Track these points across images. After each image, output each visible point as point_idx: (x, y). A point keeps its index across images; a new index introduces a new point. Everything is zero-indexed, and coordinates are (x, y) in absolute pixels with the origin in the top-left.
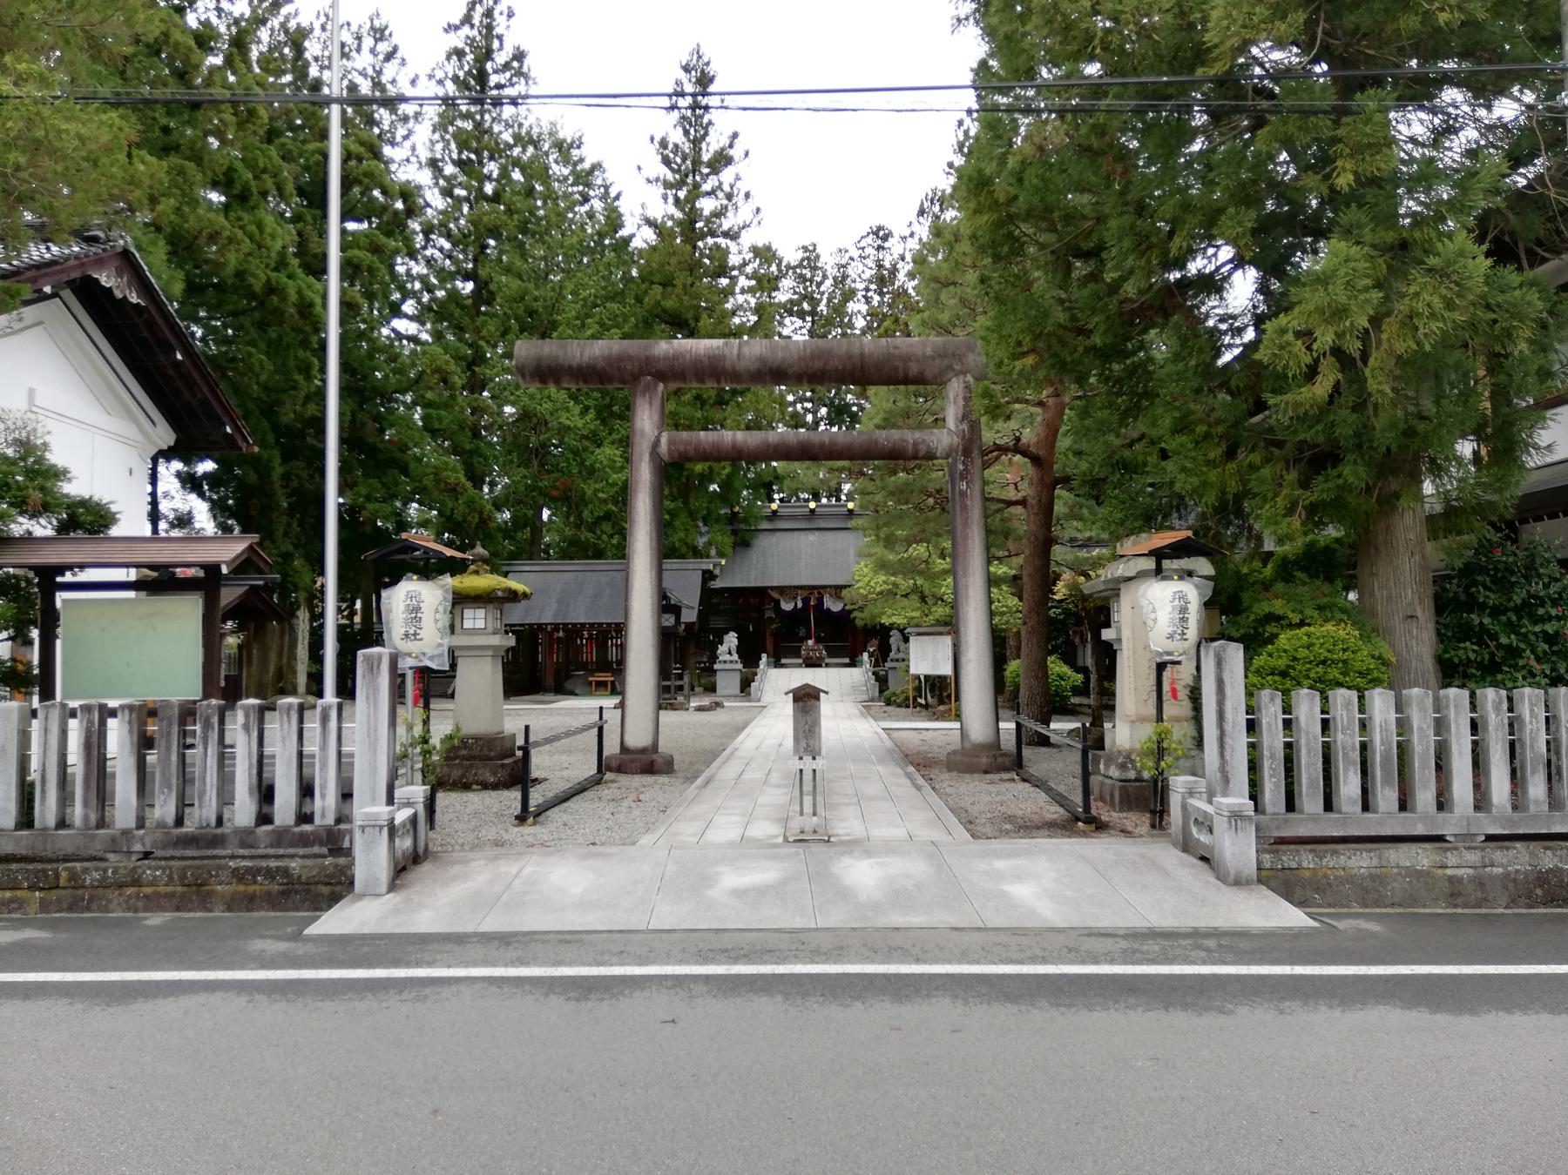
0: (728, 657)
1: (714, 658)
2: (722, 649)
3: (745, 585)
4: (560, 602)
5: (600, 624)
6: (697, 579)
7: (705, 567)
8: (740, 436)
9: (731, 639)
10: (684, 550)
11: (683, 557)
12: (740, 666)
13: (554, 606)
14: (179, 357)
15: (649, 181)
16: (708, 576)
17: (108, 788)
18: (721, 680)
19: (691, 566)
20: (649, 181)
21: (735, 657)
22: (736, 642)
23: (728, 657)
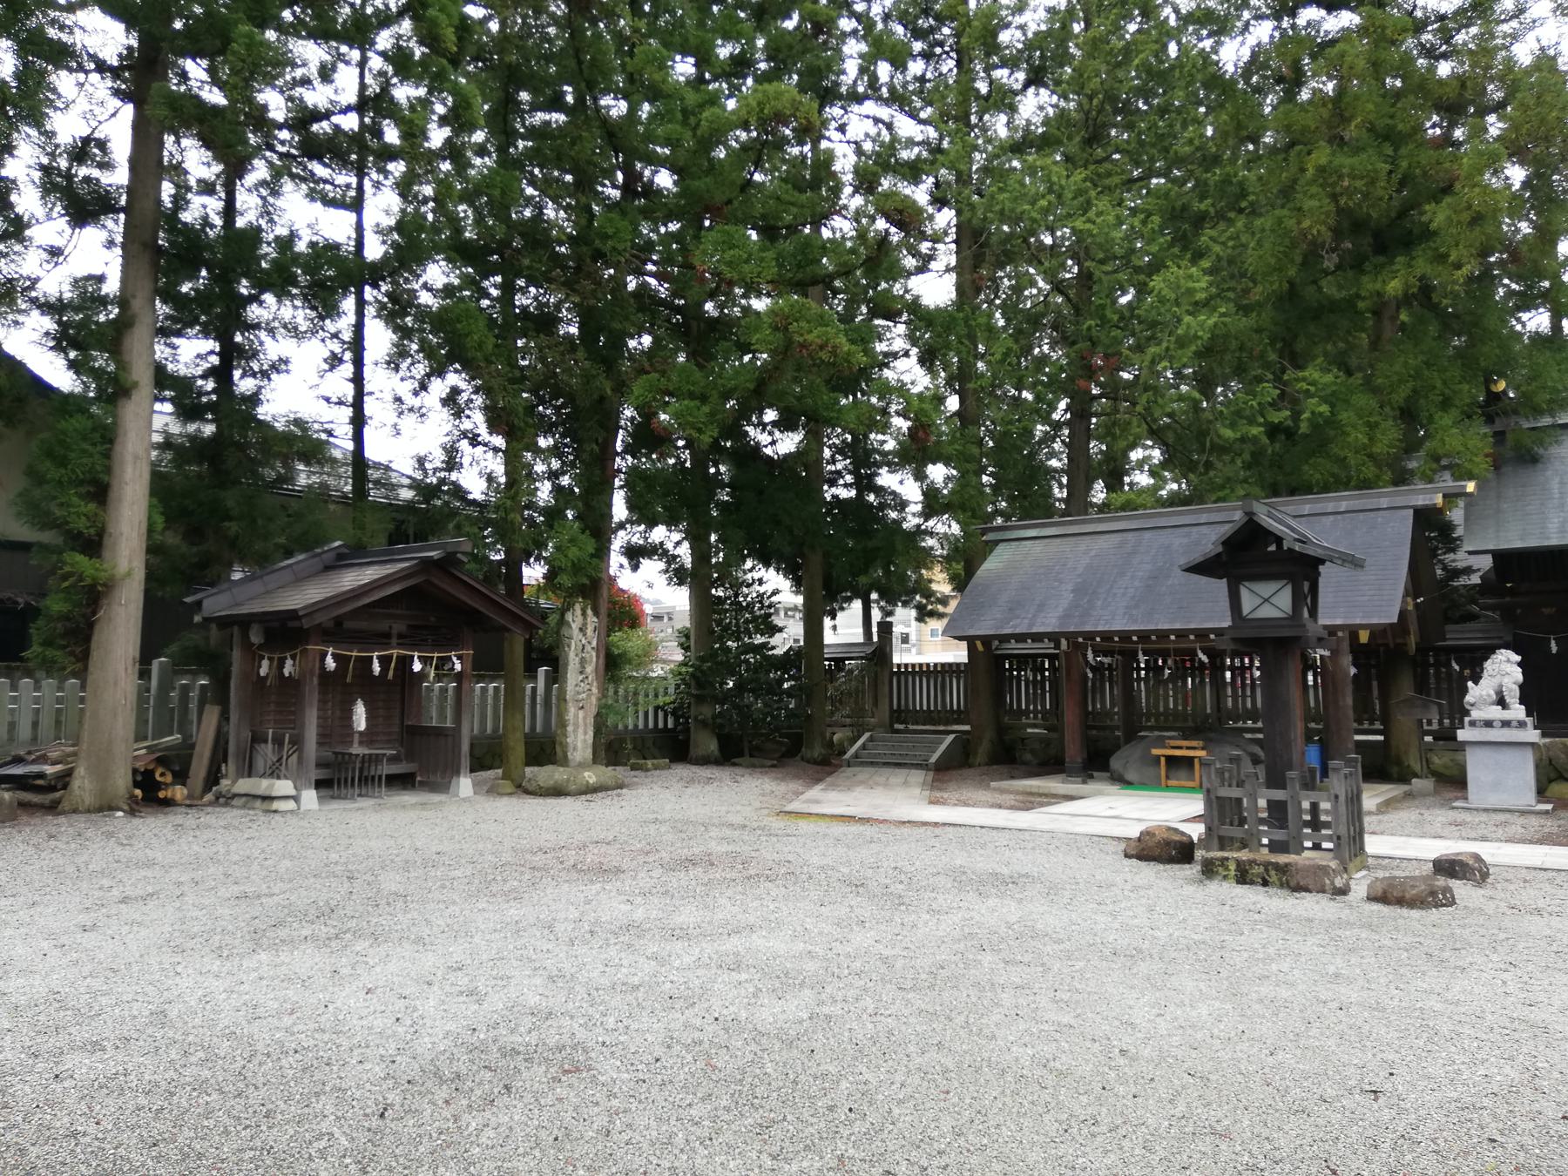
0: (1496, 713)
1: (1459, 712)
2: (1478, 693)
3: (1533, 542)
4: (1079, 591)
5: (1163, 635)
6: (1404, 525)
7: (1421, 501)
8: (120, 720)
9: (1505, 669)
10: (1370, 471)
11: (1365, 484)
12: (1533, 735)
13: (1066, 598)
14: (525, 395)
15: (328, 400)
16: (1431, 531)
17: (899, 776)
18: (1478, 767)
19: (1384, 502)
20: (328, 400)
21: (1518, 711)
22: (1518, 674)
23: (1496, 713)
